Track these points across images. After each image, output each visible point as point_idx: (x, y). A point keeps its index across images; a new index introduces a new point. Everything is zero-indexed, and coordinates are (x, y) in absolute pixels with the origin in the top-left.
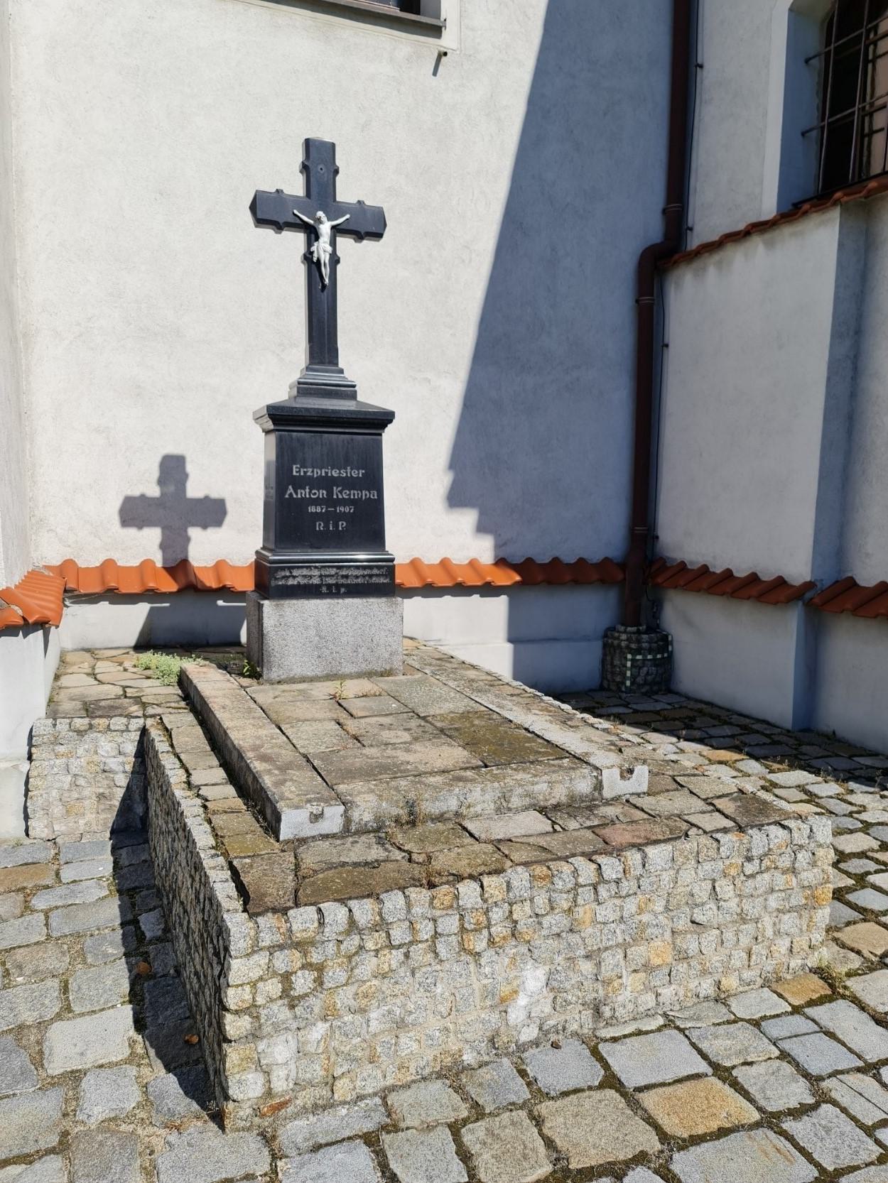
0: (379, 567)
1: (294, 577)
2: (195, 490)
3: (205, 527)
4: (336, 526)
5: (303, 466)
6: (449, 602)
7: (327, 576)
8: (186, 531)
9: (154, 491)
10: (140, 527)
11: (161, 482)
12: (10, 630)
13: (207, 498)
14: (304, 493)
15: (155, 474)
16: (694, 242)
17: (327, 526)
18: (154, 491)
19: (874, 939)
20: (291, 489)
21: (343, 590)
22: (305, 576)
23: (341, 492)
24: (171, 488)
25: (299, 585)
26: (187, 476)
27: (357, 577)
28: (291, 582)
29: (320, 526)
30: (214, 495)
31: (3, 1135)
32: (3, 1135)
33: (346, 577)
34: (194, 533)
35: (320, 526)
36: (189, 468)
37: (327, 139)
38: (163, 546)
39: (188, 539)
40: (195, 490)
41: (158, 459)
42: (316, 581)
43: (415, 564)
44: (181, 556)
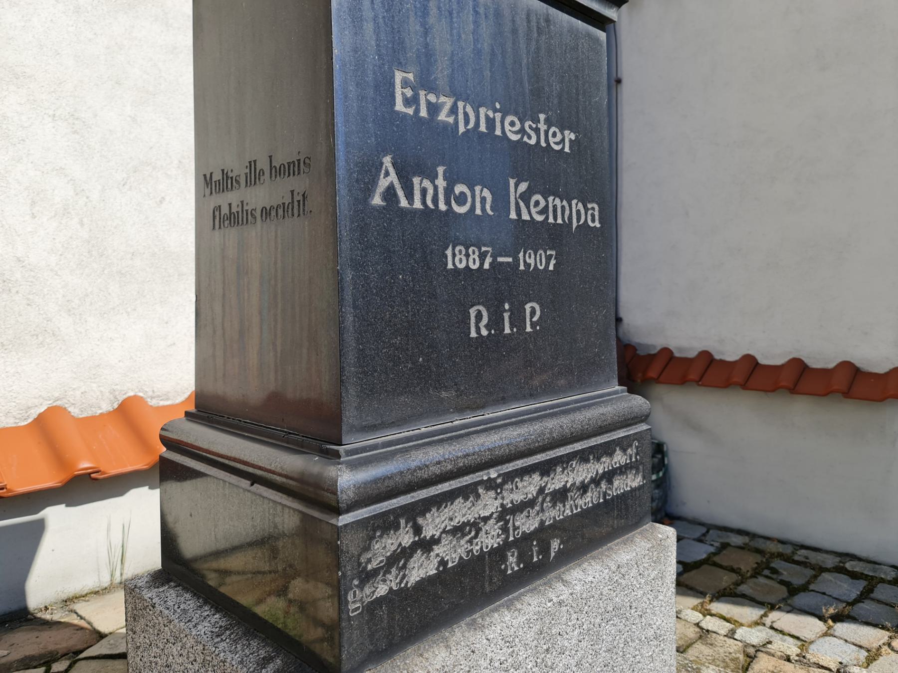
0: (623, 444)
1: (426, 545)
4: (518, 319)
5: (425, 82)
6: (801, 412)
12: (852, 384)
14: (428, 192)
17: (496, 322)
20: (389, 178)
21: (512, 562)
22: (458, 531)
23: (525, 197)
25: (446, 575)
27: (584, 488)
28: (421, 569)
29: (479, 325)
31: (729, 671)
32: (729, 671)
33: (561, 495)
35: (479, 325)
42: (490, 538)
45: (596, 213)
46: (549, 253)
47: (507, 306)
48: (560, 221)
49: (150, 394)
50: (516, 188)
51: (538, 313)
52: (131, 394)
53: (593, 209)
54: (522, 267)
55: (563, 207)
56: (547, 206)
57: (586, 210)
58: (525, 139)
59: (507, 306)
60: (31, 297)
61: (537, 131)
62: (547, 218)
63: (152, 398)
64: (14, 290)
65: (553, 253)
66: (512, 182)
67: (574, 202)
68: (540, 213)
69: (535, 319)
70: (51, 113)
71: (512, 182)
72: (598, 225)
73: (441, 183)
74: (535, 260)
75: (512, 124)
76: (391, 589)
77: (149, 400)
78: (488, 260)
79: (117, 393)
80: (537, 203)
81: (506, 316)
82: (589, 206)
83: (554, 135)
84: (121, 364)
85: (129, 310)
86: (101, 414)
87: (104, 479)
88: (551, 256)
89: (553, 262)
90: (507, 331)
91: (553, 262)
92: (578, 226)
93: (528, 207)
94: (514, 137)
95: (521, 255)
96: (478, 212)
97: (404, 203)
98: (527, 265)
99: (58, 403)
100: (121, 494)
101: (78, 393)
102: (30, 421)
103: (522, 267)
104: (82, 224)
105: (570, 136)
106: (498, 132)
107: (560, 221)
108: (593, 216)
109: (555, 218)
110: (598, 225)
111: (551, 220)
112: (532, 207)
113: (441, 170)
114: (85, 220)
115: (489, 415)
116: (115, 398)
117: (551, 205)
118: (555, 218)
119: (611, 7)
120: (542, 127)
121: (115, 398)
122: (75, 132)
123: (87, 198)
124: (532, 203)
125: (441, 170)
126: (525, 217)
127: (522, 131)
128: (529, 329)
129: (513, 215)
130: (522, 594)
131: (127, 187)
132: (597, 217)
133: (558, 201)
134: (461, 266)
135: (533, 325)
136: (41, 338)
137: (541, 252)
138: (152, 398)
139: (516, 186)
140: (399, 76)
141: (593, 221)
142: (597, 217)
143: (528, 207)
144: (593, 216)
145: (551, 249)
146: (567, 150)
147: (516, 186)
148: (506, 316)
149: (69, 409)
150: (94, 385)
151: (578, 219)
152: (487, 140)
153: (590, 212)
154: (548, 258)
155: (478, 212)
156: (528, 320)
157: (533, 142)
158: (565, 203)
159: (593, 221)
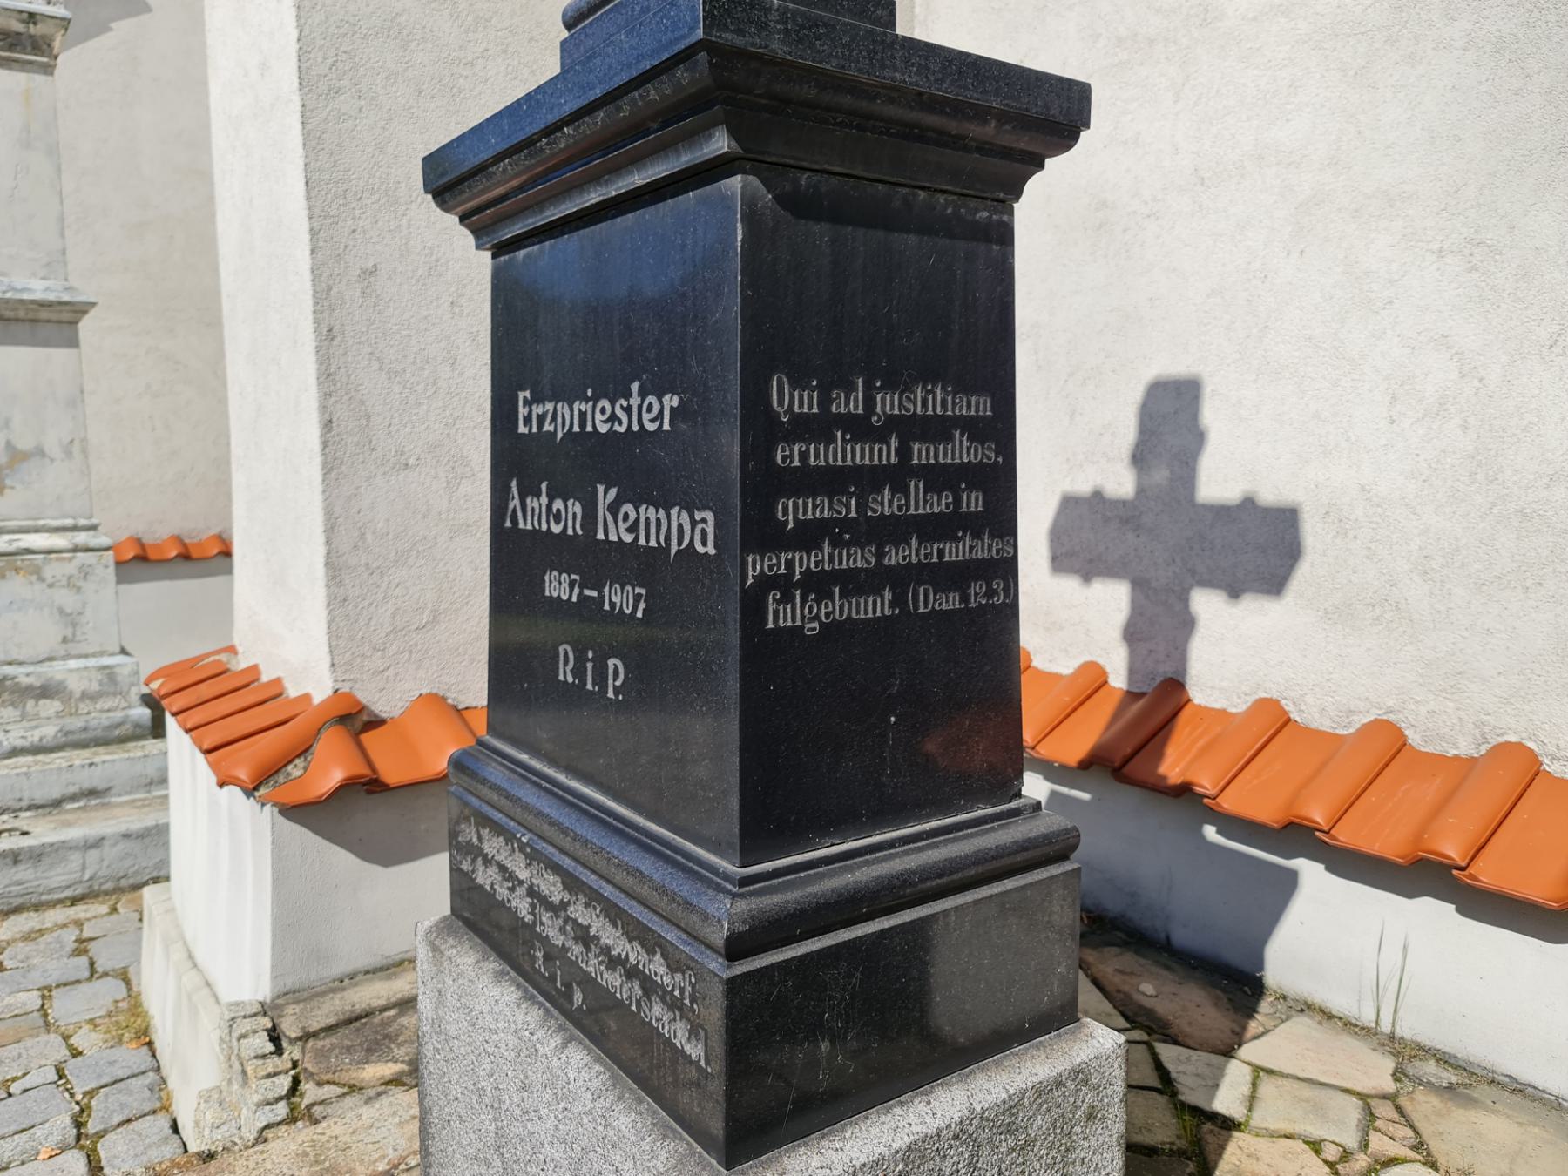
2: (1219, 480)
3: (1234, 593)
7: (783, 585)
8: (1185, 601)
9: (1121, 483)
10: (1087, 578)
11: (1140, 458)
13: (1249, 503)
15: (1127, 432)
16: (365, 771)
18: (1121, 483)
19: (605, 403)
23: (614, 508)
24: (1160, 476)
26: (1199, 437)
30: (1269, 495)
34: (1206, 604)
36: (1211, 415)
37: (1080, 77)
38: (1132, 634)
39: (1188, 624)
40: (1219, 480)
41: (1136, 394)
43: (1273, 723)
44: (1166, 670)
45: (710, 529)
46: (638, 590)
47: (590, 655)
48: (653, 543)
49: (1552, 749)
50: (605, 496)
51: (622, 676)
52: (1513, 738)
53: (704, 521)
54: (607, 607)
55: (658, 520)
56: (637, 520)
57: (694, 523)
58: (617, 428)
59: (590, 655)
60: (1372, 546)
61: (628, 410)
62: (637, 539)
63: (1554, 758)
64: (1351, 534)
65: (643, 591)
66: (601, 488)
67: (674, 512)
68: (629, 530)
69: (618, 683)
70: (1436, 246)
71: (601, 488)
72: (712, 551)
73: (544, 500)
74: (621, 598)
75: (603, 411)
76: (589, 926)
77: (1546, 761)
78: (576, 591)
79: (1486, 729)
80: (626, 517)
81: (589, 665)
82: (698, 516)
83: (650, 409)
84: (1502, 679)
85: (1529, 583)
86: (1456, 757)
87: (1334, 847)
88: (640, 595)
89: (642, 605)
90: (589, 687)
91: (642, 605)
92: (679, 551)
93: (616, 522)
94: (603, 429)
95: (606, 590)
96: (570, 532)
97: (521, 525)
98: (612, 605)
99: (1391, 717)
100: (1410, 896)
101: (1423, 710)
102: (1352, 730)
103: (607, 607)
104: (1465, 427)
105: (671, 401)
106: (589, 429)
107: (653, 543)
108: (704, 533)
109: (648, 540)
110: (712, 551)
111: (642, 542)
112: (620, 522)
113: (544, 486)
114: (1472, 420)
115: (945, 880)
116: (1483, 735)
117: (642, 520)
118: (648, 540)
119: (710, 136)
120: (635, 401)
121: (1483, 735)
122: (1474, 269)
123: (1481, 380)
124: (621, 516)
125: (544, 486)
126: (613, 538)
127: (613, 418)
128: (611, 694)
129: (600, 536)
130: (541, 1005)
131: (1556, 350)
132: (711, 537)
133: (652, 510)
134: (555, 594)
135: (617, 690)
136: (1378, 611)
137: (629, 588)
138: (1554, 758)
139: (605, 493)
140: (522, 395)
141: (704, 544)
142: (711, 537)
143: (616, 522)
144: (704, 533)
145: (641, 586)
146: (666, 427)
147: (605, 493)
148: (589, 665)
149: (1407, 733)
150: (1451, 704)
151: (680, 543)
152: (583, 440)
153: (699, 527)
154: (637, 598)
155: (570, 532)
156: (610, 681)
157: (622, 429)
158: (662, 514)
159: (704, 544)
